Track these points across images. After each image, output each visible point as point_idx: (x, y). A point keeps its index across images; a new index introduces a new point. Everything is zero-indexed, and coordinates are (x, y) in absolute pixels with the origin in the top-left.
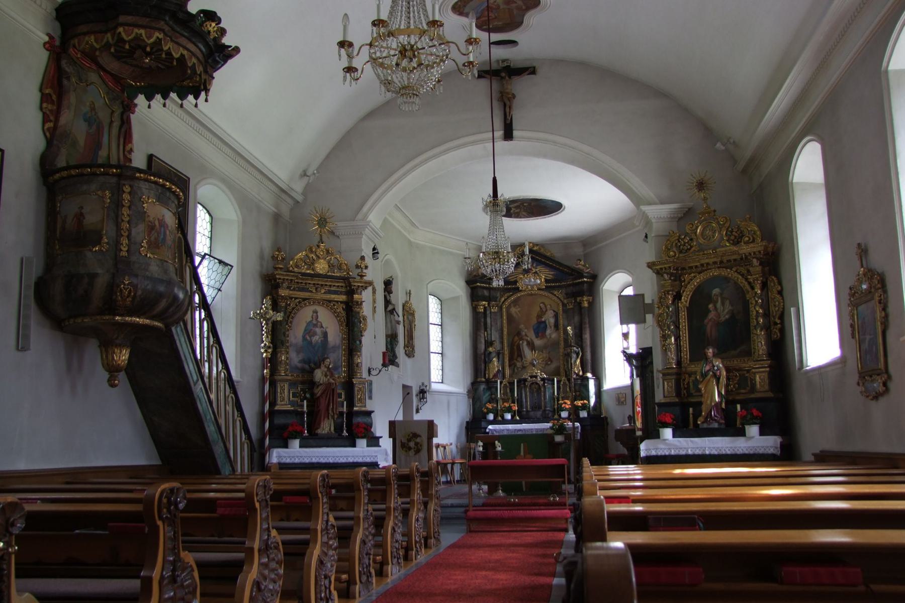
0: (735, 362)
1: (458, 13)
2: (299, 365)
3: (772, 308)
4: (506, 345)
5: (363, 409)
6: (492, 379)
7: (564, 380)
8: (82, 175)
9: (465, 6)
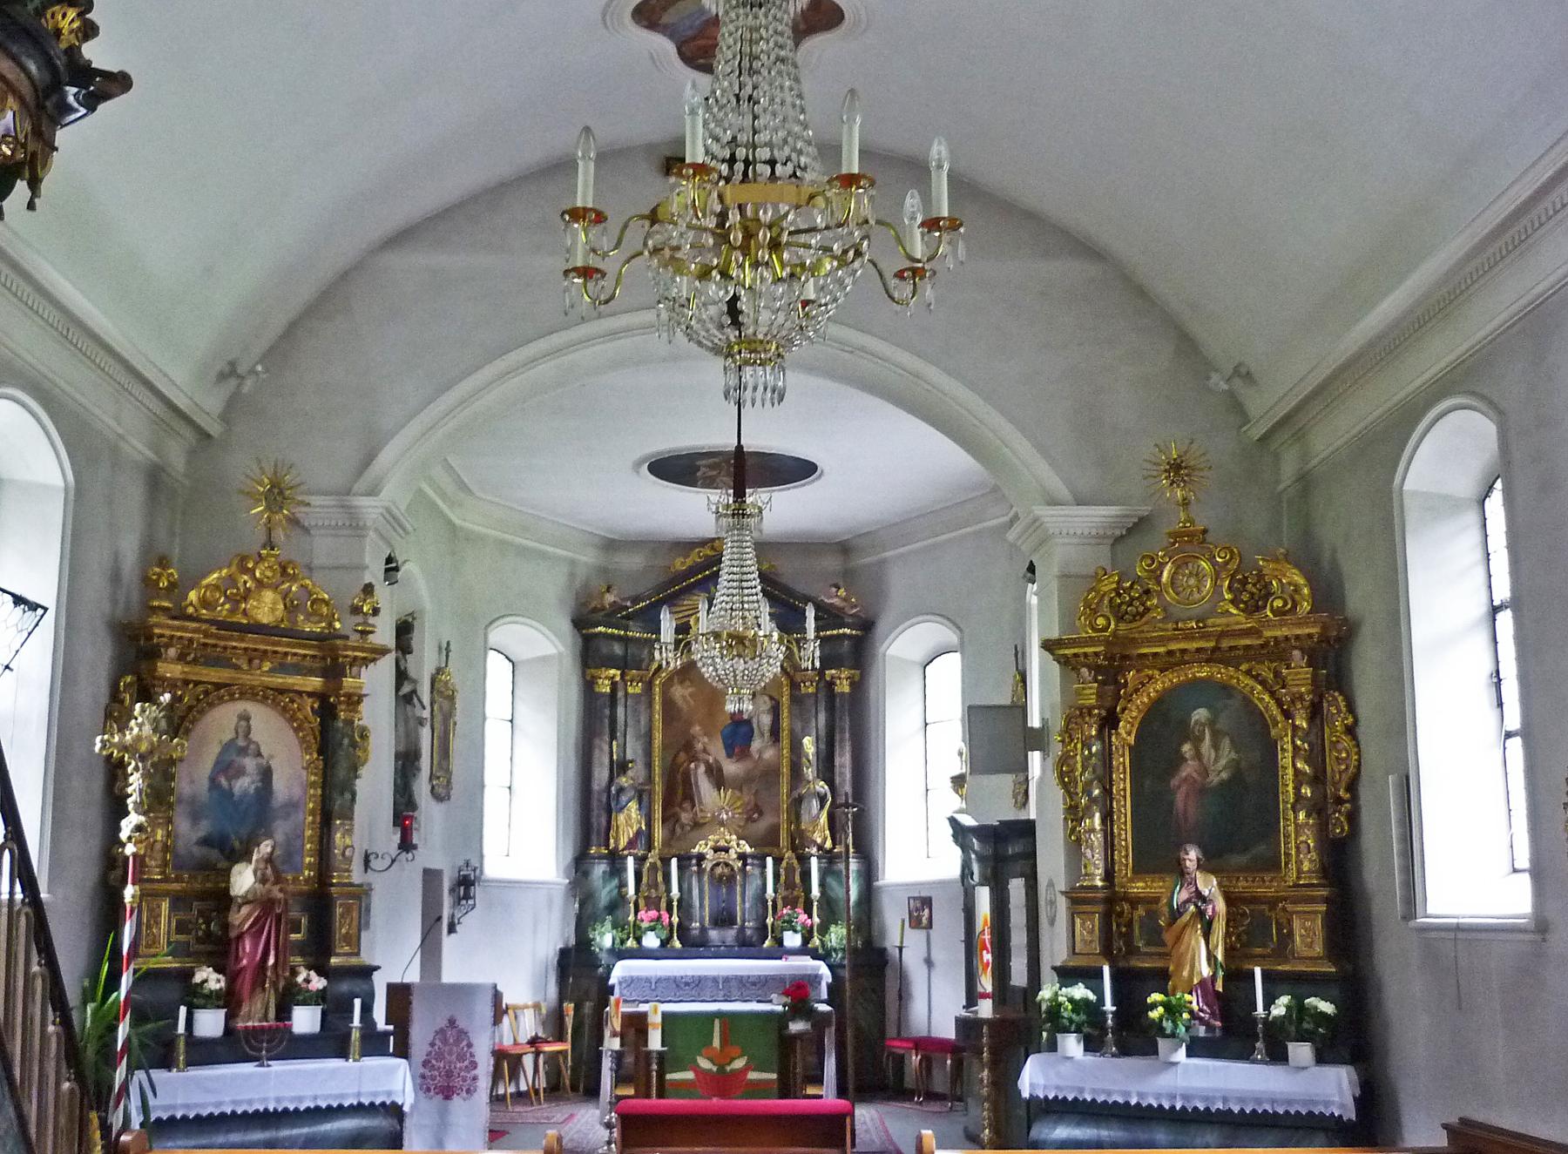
0: (1242, 883)
1: (645, 23)
2: (198, 851)
5: (354, 961)
6: (623, 850)
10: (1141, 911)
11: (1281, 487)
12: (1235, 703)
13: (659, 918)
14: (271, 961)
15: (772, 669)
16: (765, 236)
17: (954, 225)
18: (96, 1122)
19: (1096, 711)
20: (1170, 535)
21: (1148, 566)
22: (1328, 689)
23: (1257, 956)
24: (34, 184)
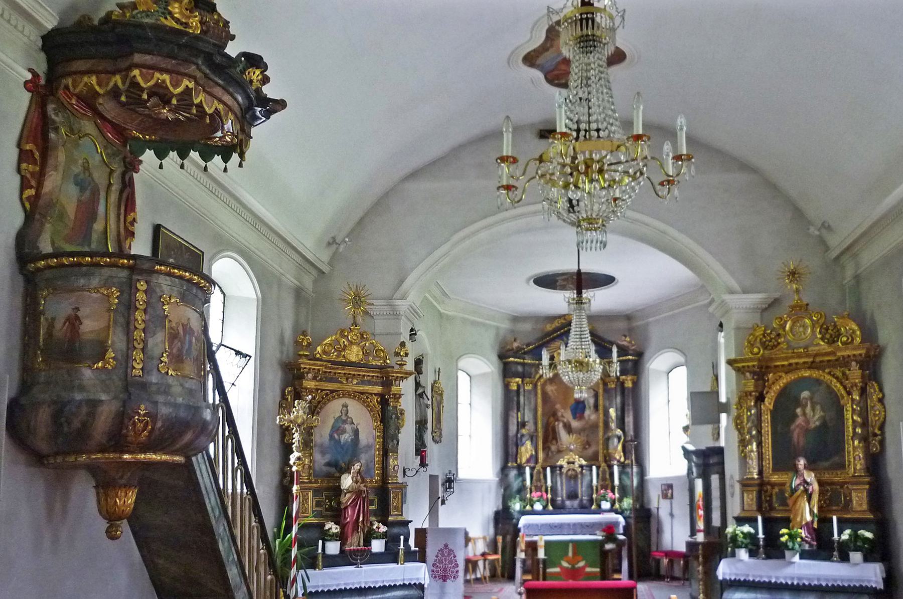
1: (528, 64)
2: (325, 469)
4: (540, 425)
5: (400, 518)
8: (79, 265)
10: (776, 490)
12: (822, 388)
13: (542, 496)
14: (361, 519)
15: (596, 376)
16: (596, 167)
17: (689, 158)
18: (282, 593)
19: (754, 393)
20: (790, 307)
21: (779, 322)
22: (870, 380)
23: (833, 510)
24: (242, 155)
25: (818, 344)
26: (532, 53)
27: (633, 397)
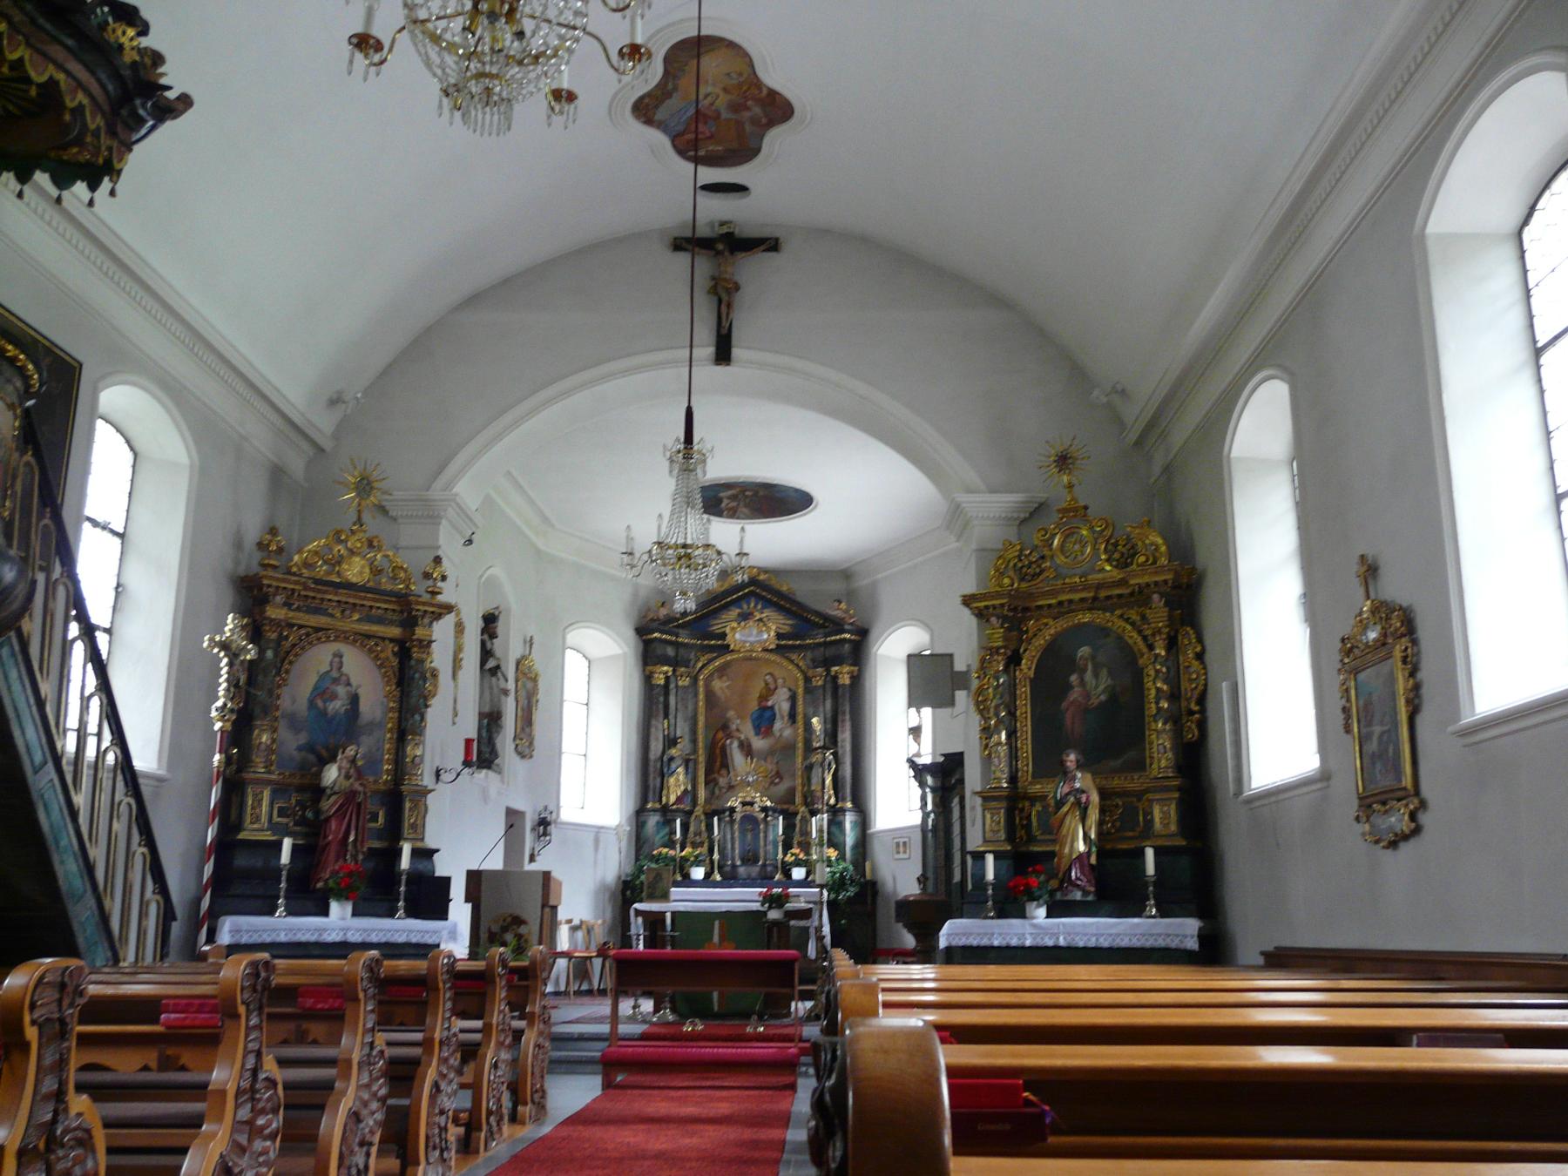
1: (643, 119)
3: (1184, 685)
4: (701, 744)
7: (803, 812)
9: (657, 107)
11: (1152, 480)
14: (352, 838)
20: (1059, 511)
22: (1182, 625)
25: (1102, 570)
26: (647, 100)
27: (850, 698)
